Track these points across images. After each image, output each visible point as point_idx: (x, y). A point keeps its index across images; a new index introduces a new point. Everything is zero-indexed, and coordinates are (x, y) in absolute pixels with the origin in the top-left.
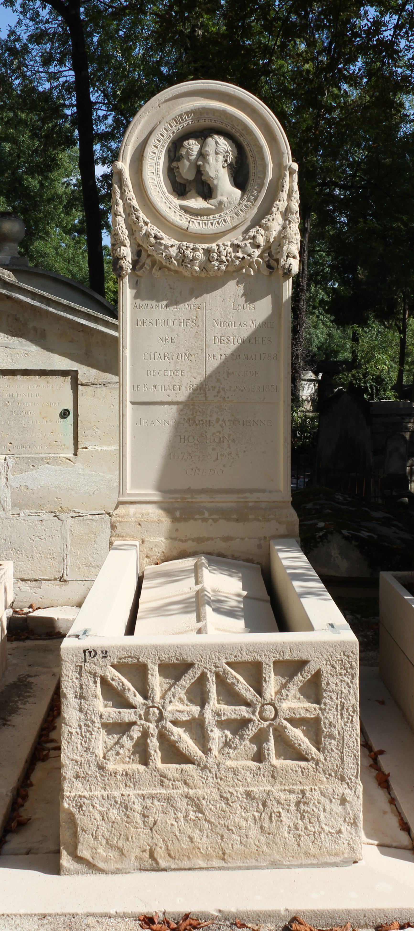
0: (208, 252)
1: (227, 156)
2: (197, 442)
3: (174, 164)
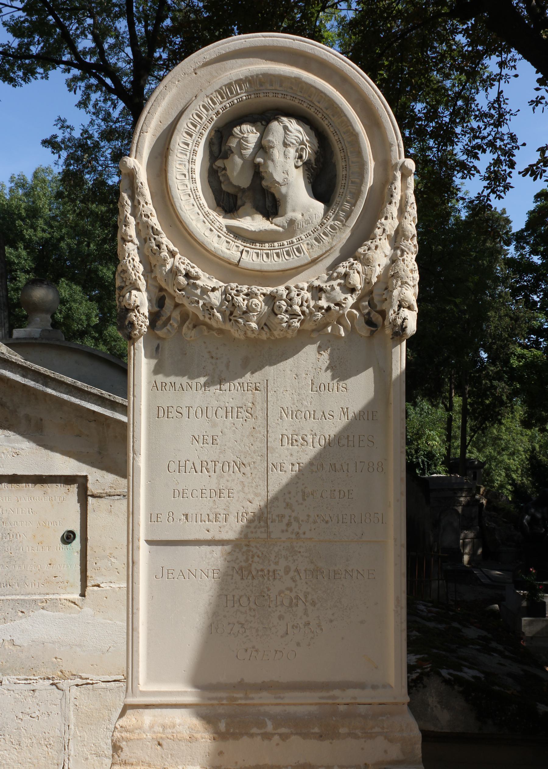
0: (271, 299)
1: (302, 149)
2: (254, 607)
3: (219, 163)
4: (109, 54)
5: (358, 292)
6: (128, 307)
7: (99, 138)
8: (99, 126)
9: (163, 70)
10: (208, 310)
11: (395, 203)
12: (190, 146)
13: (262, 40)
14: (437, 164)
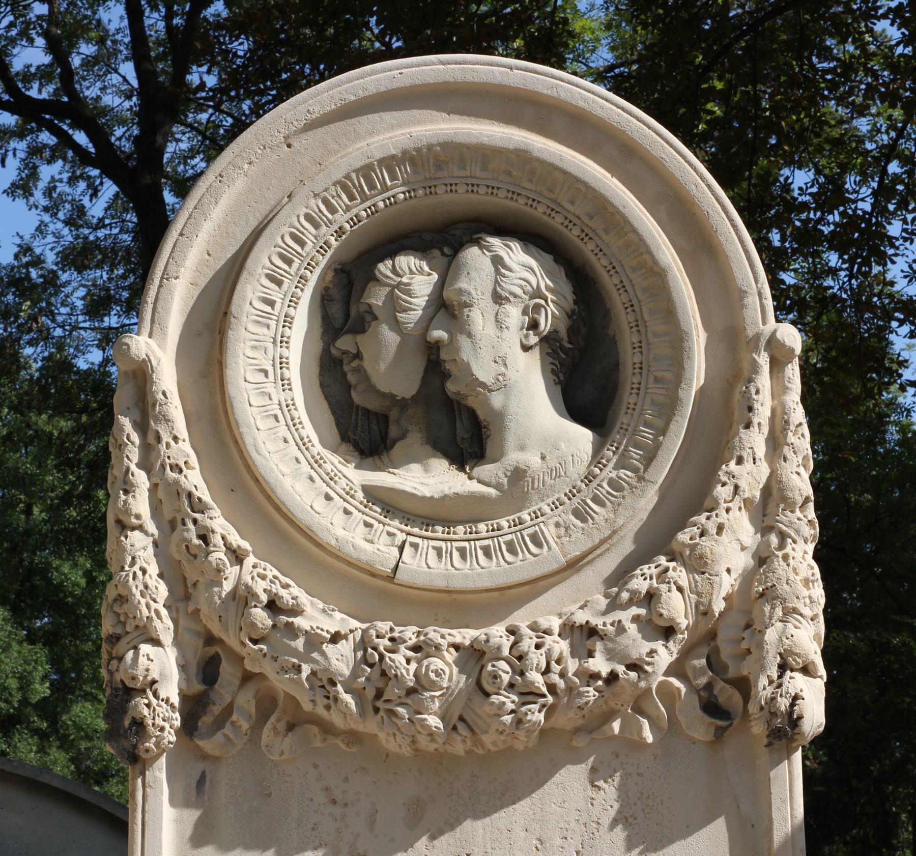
1: (537, 307)
3: (345, 343)
4: (84, 79)
5: (680, 636)
6: (130, 684)
7: (57, 264)
8: (58, 236)
9: (206, 111)
10: (323, 687)
11: (759, 424)
12: (278, 306)
13: (439, 70)
14: (851, 307)
